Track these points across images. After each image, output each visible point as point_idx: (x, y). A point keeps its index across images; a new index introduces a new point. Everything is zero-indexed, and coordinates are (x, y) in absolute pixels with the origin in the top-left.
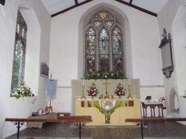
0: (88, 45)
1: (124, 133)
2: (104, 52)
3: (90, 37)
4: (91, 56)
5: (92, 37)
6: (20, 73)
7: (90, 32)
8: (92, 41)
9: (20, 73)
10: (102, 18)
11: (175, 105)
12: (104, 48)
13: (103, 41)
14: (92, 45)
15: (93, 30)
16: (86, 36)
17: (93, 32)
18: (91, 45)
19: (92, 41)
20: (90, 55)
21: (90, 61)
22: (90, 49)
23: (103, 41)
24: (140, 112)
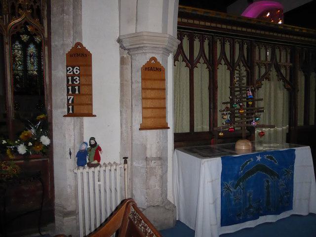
0: (14, 60)
1: (236, 200)
2: (32, 68)
3: (16, 51)
4: (19, 72)
5: (18, 51)
6: (139, 165)
7: (16, 46)
8: (19, 55)
9: (139, 165)
10: (79, 80)
11: (221, 161)
12: (33, 64)
13: (31, 56)
14: (19, 60)
15: (20, 44)
16: (12, 49)
17: (19, 46)
18: (17, 59)
19: (19, 55)
20: (17, 70)
21: (17, 77)
22: (17, 64)
23: (31, 56)
24: (124, 183)
